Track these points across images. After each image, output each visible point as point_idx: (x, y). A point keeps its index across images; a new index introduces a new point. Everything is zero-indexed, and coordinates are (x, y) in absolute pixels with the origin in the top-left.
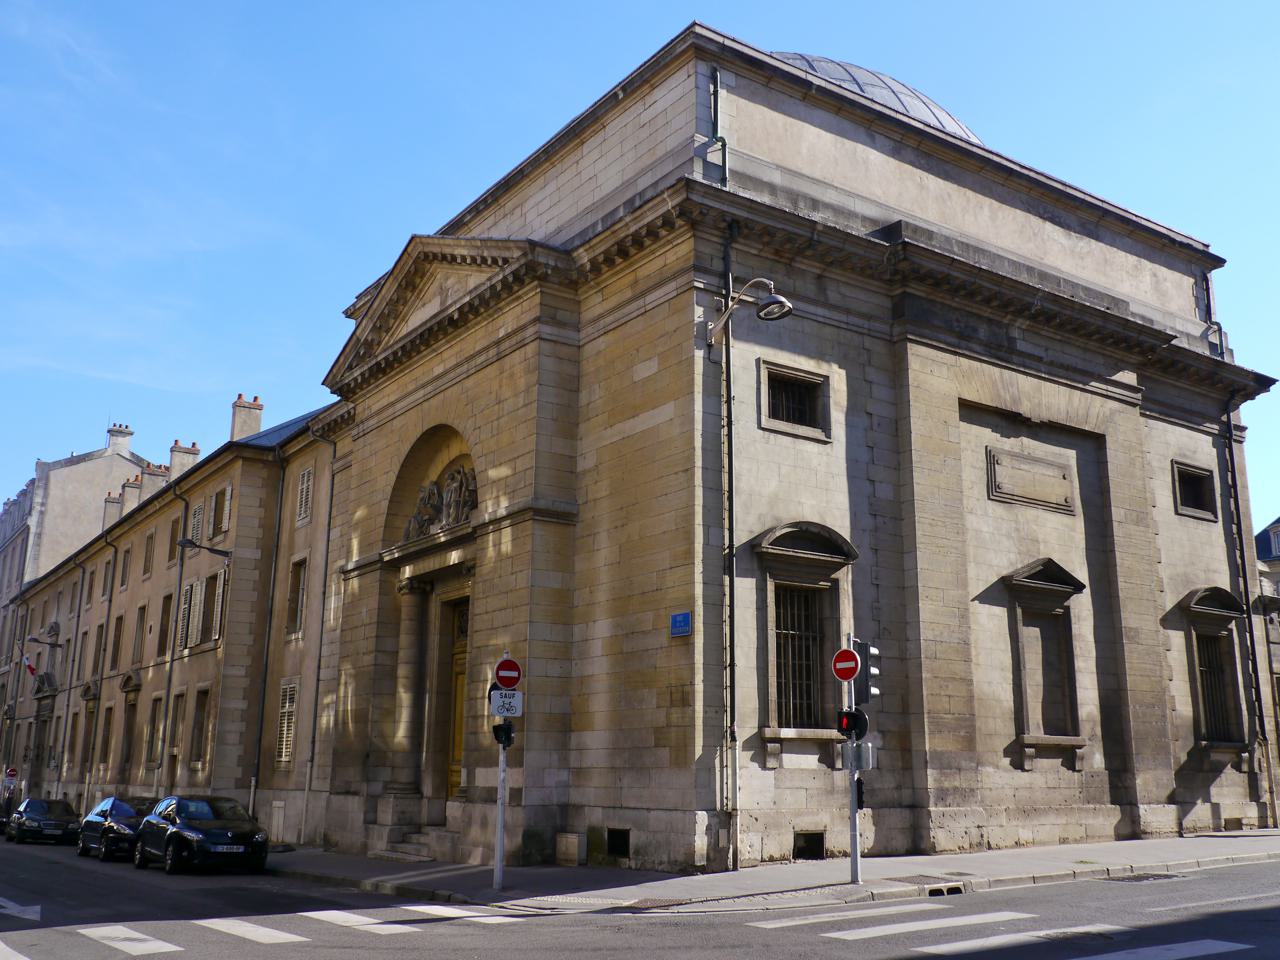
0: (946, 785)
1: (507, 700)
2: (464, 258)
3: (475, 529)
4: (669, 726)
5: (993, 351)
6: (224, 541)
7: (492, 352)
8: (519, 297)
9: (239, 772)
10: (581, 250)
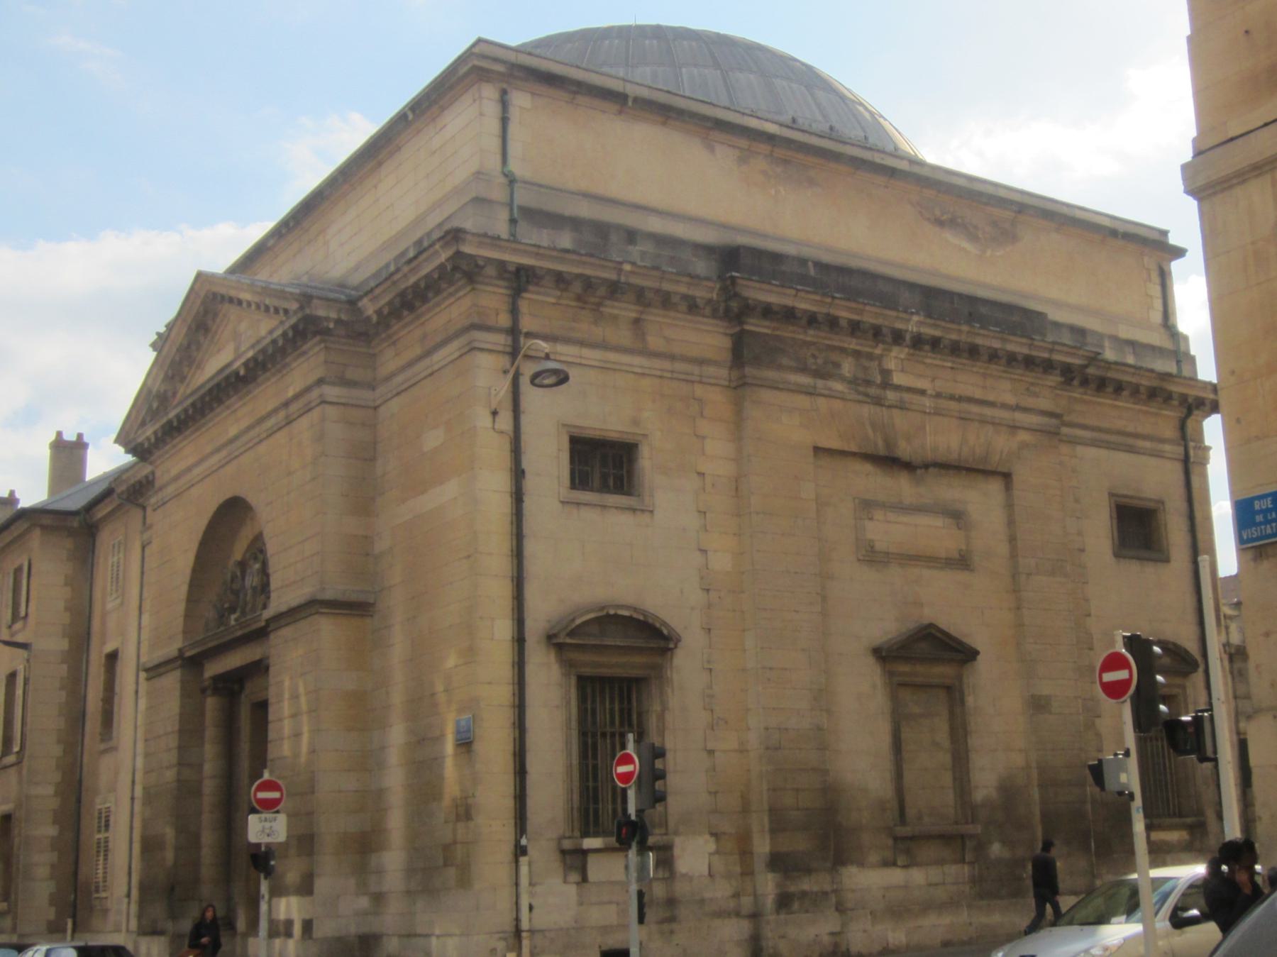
0: (792, 889)
1: (267, 825)
2: (249, 304)
3: (268, 621)
4: (455, 842)
5: (861, 389)
6: (25, 626)
7: (282, 414)
8: (305, 353)
9: (51, 914)
10: (365, 300)
